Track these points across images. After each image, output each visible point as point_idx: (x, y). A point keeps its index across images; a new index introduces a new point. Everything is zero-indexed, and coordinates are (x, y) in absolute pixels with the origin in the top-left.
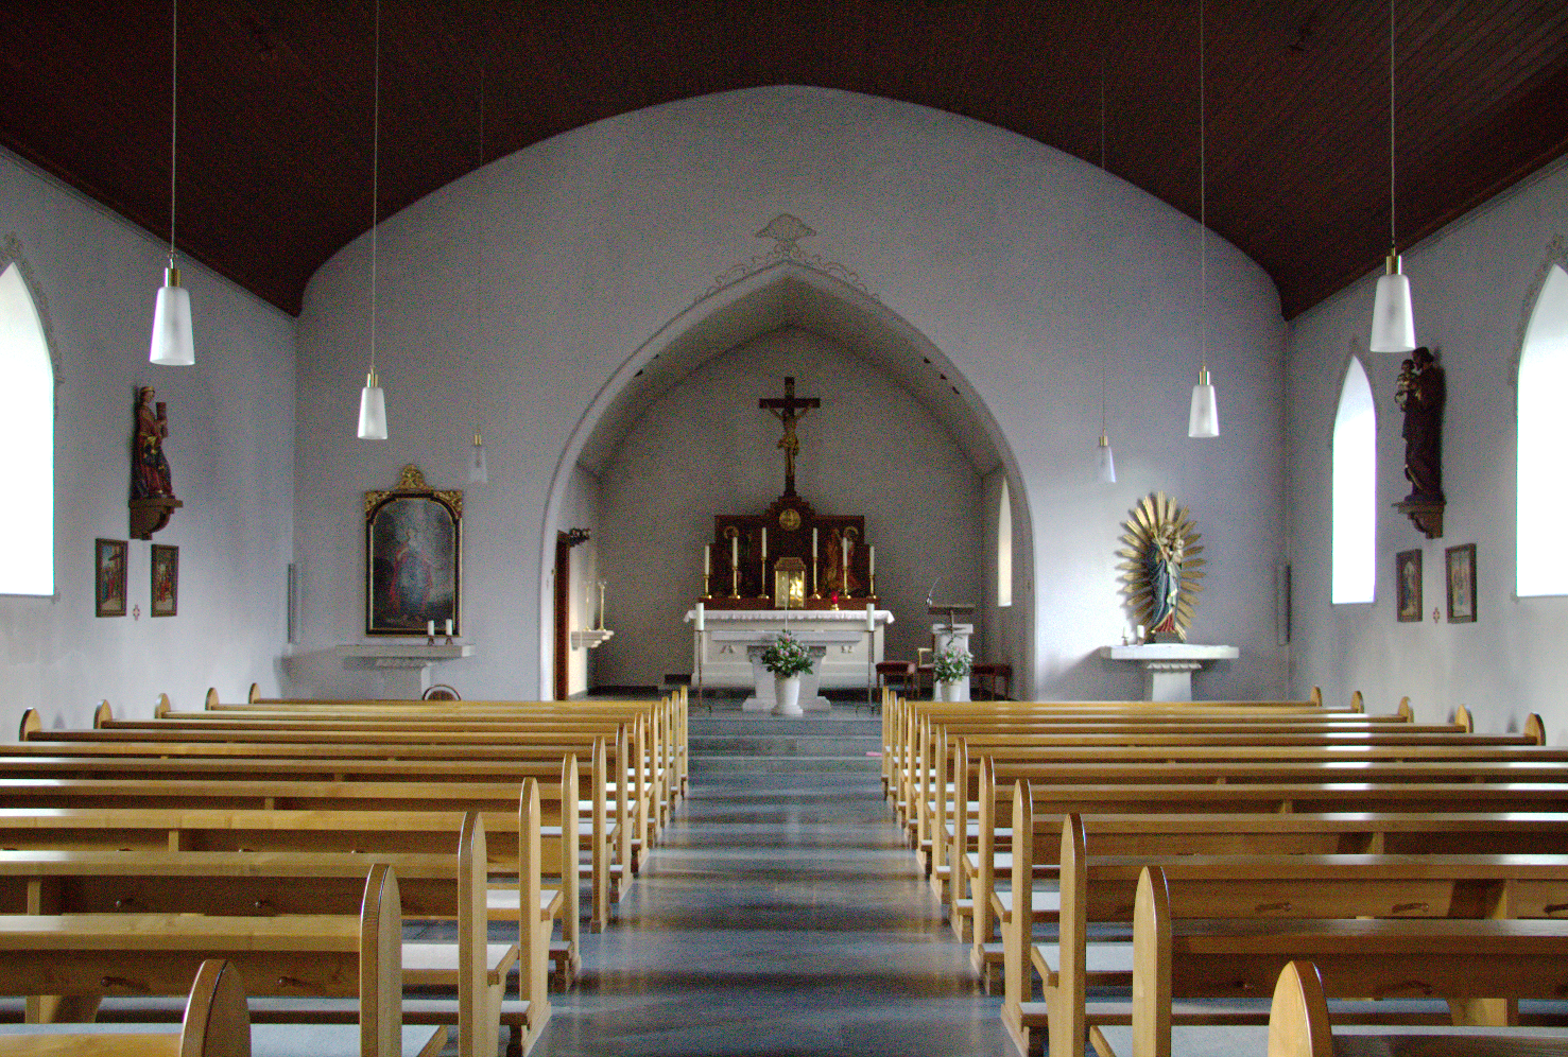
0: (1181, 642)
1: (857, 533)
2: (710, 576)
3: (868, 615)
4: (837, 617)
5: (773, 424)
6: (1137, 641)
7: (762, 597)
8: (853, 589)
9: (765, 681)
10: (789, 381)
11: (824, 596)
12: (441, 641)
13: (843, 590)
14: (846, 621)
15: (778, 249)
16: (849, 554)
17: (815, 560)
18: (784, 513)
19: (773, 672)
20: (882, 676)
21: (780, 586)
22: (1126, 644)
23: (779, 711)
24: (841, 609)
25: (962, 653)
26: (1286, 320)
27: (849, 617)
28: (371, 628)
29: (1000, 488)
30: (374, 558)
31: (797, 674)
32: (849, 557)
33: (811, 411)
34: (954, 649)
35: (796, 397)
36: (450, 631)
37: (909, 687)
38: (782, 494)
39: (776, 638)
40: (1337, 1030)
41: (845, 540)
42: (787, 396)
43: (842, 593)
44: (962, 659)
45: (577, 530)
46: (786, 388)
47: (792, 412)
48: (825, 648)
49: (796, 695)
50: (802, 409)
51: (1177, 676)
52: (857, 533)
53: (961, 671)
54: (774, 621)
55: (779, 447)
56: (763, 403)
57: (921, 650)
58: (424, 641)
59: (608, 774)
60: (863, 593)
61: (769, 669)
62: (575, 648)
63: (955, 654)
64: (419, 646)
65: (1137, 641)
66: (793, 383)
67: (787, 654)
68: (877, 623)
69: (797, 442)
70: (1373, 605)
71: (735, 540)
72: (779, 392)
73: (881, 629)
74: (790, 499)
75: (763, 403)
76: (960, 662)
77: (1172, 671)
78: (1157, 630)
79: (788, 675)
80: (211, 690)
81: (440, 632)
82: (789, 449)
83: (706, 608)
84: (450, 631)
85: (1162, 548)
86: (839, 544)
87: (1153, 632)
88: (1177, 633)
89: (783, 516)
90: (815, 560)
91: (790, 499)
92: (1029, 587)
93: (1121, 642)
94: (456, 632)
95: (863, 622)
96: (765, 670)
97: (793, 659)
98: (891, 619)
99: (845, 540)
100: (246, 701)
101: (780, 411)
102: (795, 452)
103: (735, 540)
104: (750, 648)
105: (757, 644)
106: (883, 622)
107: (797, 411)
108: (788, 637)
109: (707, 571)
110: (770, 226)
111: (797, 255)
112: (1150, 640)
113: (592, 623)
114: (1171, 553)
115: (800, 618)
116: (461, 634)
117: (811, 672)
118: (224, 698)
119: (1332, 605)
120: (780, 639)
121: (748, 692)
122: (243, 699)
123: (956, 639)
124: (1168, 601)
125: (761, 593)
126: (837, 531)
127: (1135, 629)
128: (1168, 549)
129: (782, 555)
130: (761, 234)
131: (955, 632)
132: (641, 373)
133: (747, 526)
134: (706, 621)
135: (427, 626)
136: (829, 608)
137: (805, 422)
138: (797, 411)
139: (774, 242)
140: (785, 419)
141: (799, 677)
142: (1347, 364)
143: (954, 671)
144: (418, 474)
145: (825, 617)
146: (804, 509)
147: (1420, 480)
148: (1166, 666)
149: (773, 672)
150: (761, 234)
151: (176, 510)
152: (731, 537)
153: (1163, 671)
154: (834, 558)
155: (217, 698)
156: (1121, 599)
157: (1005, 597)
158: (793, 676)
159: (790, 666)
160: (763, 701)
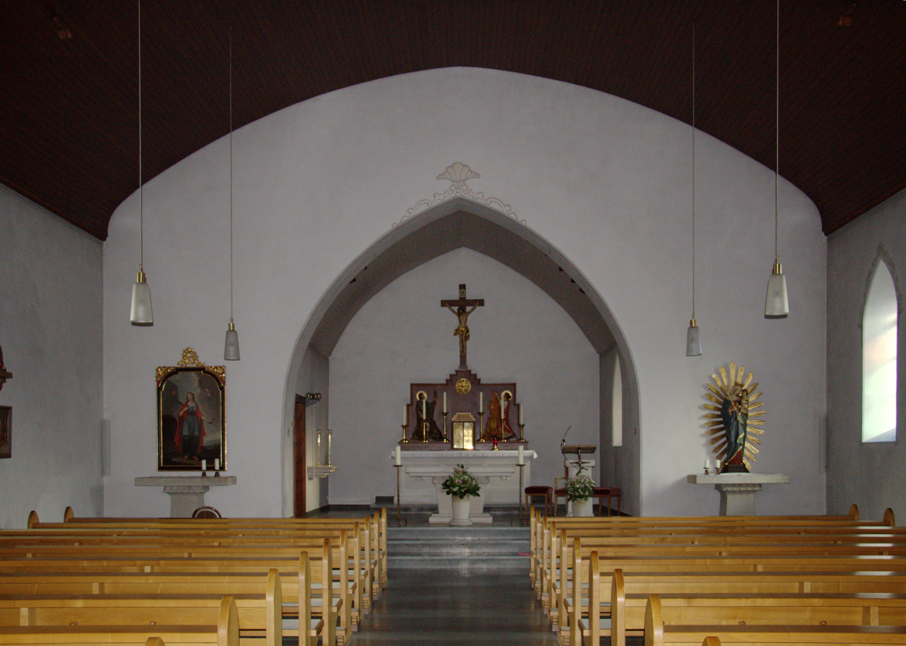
0: (747, 471)
1: (511, 394)
2: (471, 536)
3: (519, 454)
4: (497, 455)
5: (451, 318)
6: (718, 471)
9: (444, 500)
10: (462, 287)
12: (211, 474)
13: (502, 435)
14: (503, 458)
15: (453, 188)
19: (451, 494)
20: (529, 497)
22: (707, 472)
25: (588, 480)
26: (826, 234)
27: (506, 455)
28: (162, 465)
29: (613, 366)
30: (163, 415)
33: (478, 308)
34: (582, 477)
36: (217, 467)
37: (549, 506)
40: (141, 281)
42: (460, 298)
44: (588, 485)
45: (310, 394)
47: (464, 310)
49: (466, 509)
50: (472, 307)
51: (744, 496)
53: (587, 493)
56: (444, 303)
58: (199, 474)
61: (448, 493)
62: (310, 479)
63: (582, 481)
64: (194, 477)
65: (718, 471)
67: (461, 482)
68: (525, 458)
69: (468, 331)
70: (895, 443)
72: (455, 295)
73: (528, 464)
74: (464, 372)
75: (444, 303)
76: (586, 487)
77: (741, 492)
78: (729, 463)
79: (462, 497)
80: (68, 508)
81: (211, 468)
82: (462, 335)
83: (402, 449)
84: (217, 467)
85: (733, 403)
87: (726, 464)
88: (744, 465)
91: (464, 372)
92: (635, 433)
93: (703, 471)
94: (222, 468)
95: (517, 458)
96: (445, 493)
97: (466, 485)
98: (535, 456)
100: (62, 521)
101: (456, 309)
102: (467, 338)
106: (531, 457)
107: (468, 309)
110: (446, 171)
111: (466, 192)
112: (725, 469)
113: (323, 460)
114: (740, 406)
116: (226, 469)
117: (478, 495)
118: (42, 519)
119: (862, 444)
121: (434, 509)
122: (59, 518)
123: (583, 471)
124: (738, 441)
127: (713, 462)
128: (737, 405)
129: (457, 412)
130: (440, 177)
131: (582, 465)
132: (354, 280)
133: (433, 389)
134: (402, 458)
135: (201, 464)
137: (475, 317)
138: (468, 309)
139: (450, 183)
140: (459, 314)
142: (874, 265)
143: (582, 493)
144: (195, 356)
145: (489, 455)
146: (474, 379)
147: (468, 457)
148: (736, 489)
149: (451, 494)
150: (440, 177)
151: (7, 380)
153: (734, 492)
155: (38, 519)
156: (703, 441)
157: (617, 439)
159: (463, 491)
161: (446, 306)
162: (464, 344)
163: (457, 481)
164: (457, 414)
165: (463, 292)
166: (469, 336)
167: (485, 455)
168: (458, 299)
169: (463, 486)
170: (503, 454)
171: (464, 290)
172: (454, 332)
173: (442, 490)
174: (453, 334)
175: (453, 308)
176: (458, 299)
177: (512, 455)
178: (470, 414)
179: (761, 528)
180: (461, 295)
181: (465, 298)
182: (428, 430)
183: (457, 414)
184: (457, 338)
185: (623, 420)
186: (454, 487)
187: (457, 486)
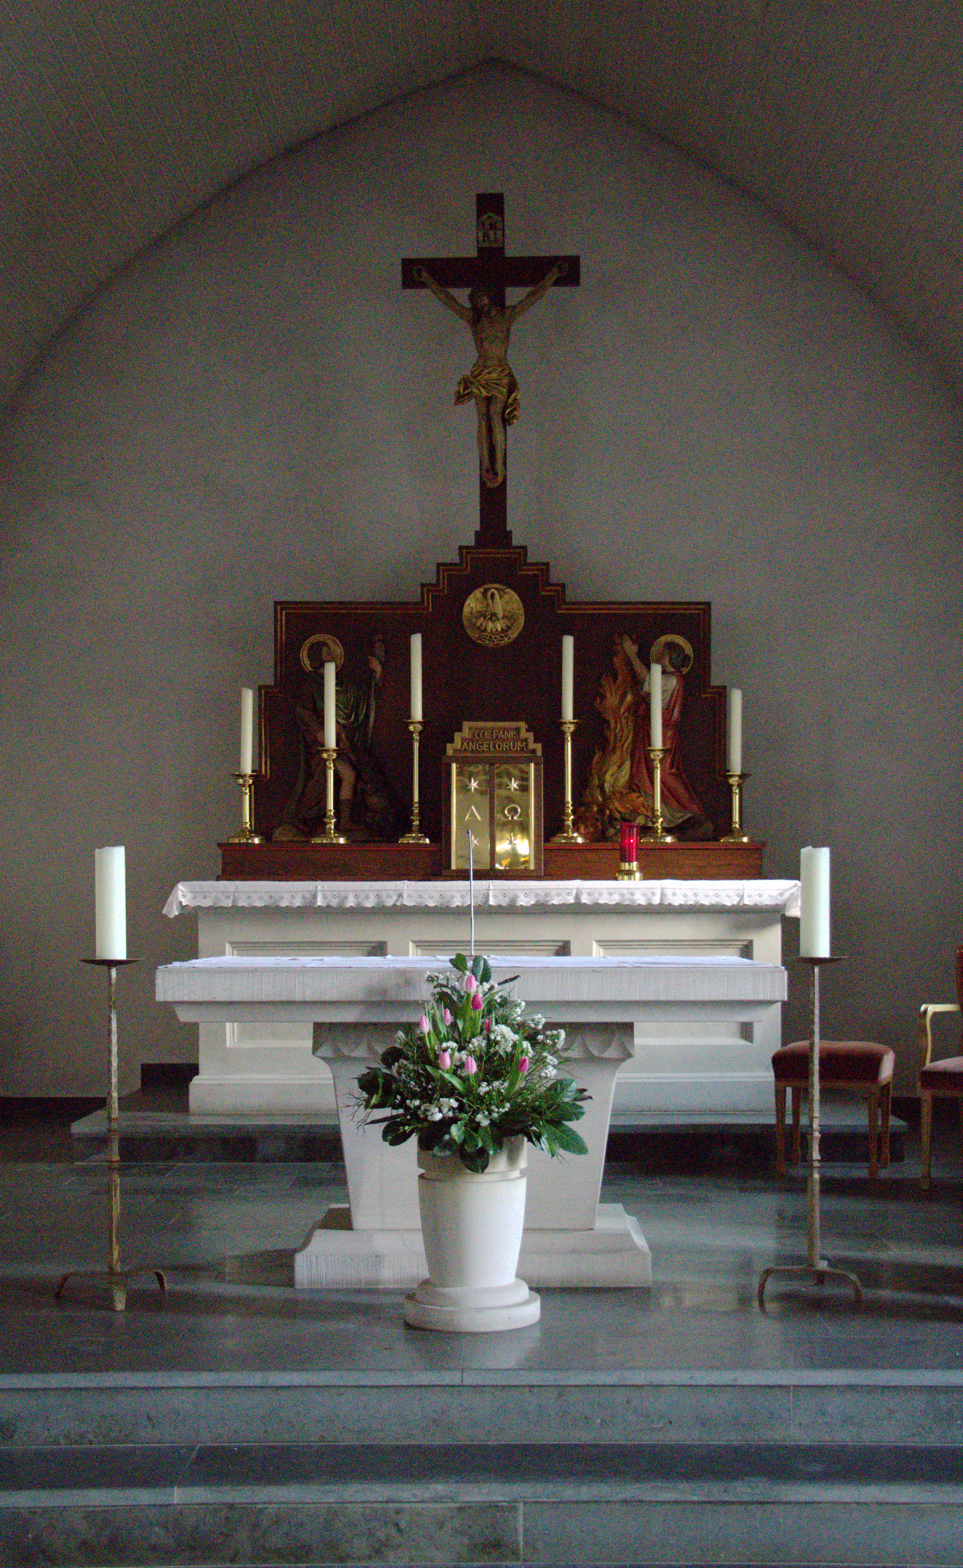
1: (688, 649)
2: (257, 776)
7: (410, 839)
8: (681, 817)
11: (598, 836)
13: (654, 818)
14: (664, 911)
16: (667, 712)
17: (569, 729)
18: (478, 593)
21: (600, 1174)
23: (438, 1315)
24: (649, 873)
27: (677, 901)
31: (513, 1158)
32: (666, 724)
33: (554, 293)
35: (510, 252)
38: (469, 540)
39: (426, 992)
41: (657, 669)
43: (646, 830)
46: (480, 225)
47: (499, 301)
48: (627, 1028)
52: (688, 649)
54: (444, 912)
55: (460, 398)
57: (932, 1008)
59: (332, 1026)
60: (708, 827)
66: (501, 212)
69: (512, 387)
71: (330, 671)
82: (489, 400)
86: (637, 684)
89: (472, 603)
90: (569, 729)
99: (657, 669)
101: (462, 295)
103: (330, 671)
104: (322, 1032)
105: (349, 1016)
107: (514, 295)
108: (477, 989)
109: (247, 766)
115: (523, 901)
120: (443, 999)
125: (408, 828)
126: (631, 648)
136: (612, 873)
138: (514, 295)
140: (477, 317)
141: (523, 1163)
152: (319, 666)
154: (623, 732)
158: (500, 1163)
160: (381, 1243)
161: (423, 285)
162: (498, 436)
163: (447, 1061)
164: (466, 725)
165: (493, 227)
166: (516, 404)
167: (585, 900)
168: (473, 253)
169: (484, 1088)
170: (663, 895)
171: (496, 218)
172: (454, 388)
173: (362, 1113)
174: (453, 398)
175: (453, 291)
176: (473, 253)
177: (706, 902)
178: (523, 725)
179: (488, 948)
180: (485, 235)
181: (502, 249)
182: (346, 794)
183: (466, 725)
184: (470, 411)
185: (719, 879)
186: (428, 1097)
187: (451, 1092)
